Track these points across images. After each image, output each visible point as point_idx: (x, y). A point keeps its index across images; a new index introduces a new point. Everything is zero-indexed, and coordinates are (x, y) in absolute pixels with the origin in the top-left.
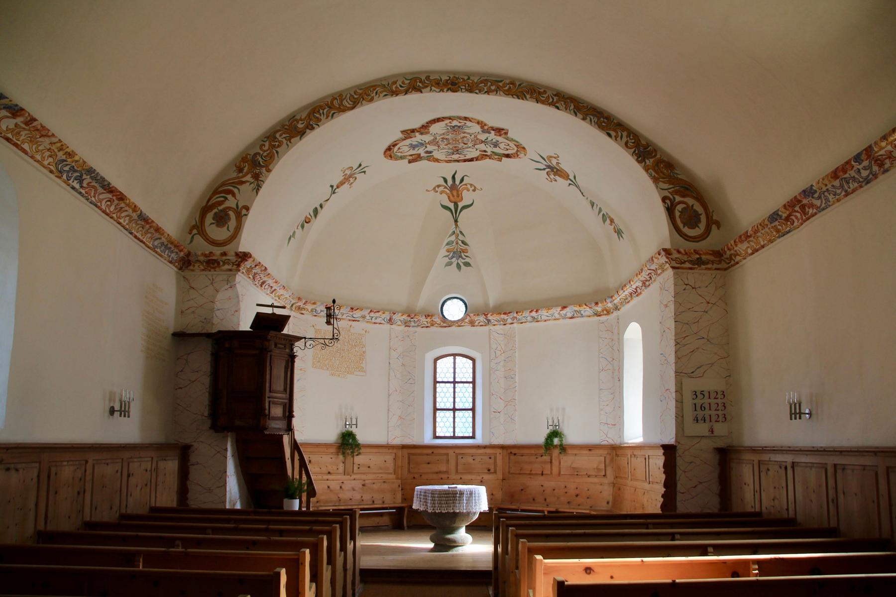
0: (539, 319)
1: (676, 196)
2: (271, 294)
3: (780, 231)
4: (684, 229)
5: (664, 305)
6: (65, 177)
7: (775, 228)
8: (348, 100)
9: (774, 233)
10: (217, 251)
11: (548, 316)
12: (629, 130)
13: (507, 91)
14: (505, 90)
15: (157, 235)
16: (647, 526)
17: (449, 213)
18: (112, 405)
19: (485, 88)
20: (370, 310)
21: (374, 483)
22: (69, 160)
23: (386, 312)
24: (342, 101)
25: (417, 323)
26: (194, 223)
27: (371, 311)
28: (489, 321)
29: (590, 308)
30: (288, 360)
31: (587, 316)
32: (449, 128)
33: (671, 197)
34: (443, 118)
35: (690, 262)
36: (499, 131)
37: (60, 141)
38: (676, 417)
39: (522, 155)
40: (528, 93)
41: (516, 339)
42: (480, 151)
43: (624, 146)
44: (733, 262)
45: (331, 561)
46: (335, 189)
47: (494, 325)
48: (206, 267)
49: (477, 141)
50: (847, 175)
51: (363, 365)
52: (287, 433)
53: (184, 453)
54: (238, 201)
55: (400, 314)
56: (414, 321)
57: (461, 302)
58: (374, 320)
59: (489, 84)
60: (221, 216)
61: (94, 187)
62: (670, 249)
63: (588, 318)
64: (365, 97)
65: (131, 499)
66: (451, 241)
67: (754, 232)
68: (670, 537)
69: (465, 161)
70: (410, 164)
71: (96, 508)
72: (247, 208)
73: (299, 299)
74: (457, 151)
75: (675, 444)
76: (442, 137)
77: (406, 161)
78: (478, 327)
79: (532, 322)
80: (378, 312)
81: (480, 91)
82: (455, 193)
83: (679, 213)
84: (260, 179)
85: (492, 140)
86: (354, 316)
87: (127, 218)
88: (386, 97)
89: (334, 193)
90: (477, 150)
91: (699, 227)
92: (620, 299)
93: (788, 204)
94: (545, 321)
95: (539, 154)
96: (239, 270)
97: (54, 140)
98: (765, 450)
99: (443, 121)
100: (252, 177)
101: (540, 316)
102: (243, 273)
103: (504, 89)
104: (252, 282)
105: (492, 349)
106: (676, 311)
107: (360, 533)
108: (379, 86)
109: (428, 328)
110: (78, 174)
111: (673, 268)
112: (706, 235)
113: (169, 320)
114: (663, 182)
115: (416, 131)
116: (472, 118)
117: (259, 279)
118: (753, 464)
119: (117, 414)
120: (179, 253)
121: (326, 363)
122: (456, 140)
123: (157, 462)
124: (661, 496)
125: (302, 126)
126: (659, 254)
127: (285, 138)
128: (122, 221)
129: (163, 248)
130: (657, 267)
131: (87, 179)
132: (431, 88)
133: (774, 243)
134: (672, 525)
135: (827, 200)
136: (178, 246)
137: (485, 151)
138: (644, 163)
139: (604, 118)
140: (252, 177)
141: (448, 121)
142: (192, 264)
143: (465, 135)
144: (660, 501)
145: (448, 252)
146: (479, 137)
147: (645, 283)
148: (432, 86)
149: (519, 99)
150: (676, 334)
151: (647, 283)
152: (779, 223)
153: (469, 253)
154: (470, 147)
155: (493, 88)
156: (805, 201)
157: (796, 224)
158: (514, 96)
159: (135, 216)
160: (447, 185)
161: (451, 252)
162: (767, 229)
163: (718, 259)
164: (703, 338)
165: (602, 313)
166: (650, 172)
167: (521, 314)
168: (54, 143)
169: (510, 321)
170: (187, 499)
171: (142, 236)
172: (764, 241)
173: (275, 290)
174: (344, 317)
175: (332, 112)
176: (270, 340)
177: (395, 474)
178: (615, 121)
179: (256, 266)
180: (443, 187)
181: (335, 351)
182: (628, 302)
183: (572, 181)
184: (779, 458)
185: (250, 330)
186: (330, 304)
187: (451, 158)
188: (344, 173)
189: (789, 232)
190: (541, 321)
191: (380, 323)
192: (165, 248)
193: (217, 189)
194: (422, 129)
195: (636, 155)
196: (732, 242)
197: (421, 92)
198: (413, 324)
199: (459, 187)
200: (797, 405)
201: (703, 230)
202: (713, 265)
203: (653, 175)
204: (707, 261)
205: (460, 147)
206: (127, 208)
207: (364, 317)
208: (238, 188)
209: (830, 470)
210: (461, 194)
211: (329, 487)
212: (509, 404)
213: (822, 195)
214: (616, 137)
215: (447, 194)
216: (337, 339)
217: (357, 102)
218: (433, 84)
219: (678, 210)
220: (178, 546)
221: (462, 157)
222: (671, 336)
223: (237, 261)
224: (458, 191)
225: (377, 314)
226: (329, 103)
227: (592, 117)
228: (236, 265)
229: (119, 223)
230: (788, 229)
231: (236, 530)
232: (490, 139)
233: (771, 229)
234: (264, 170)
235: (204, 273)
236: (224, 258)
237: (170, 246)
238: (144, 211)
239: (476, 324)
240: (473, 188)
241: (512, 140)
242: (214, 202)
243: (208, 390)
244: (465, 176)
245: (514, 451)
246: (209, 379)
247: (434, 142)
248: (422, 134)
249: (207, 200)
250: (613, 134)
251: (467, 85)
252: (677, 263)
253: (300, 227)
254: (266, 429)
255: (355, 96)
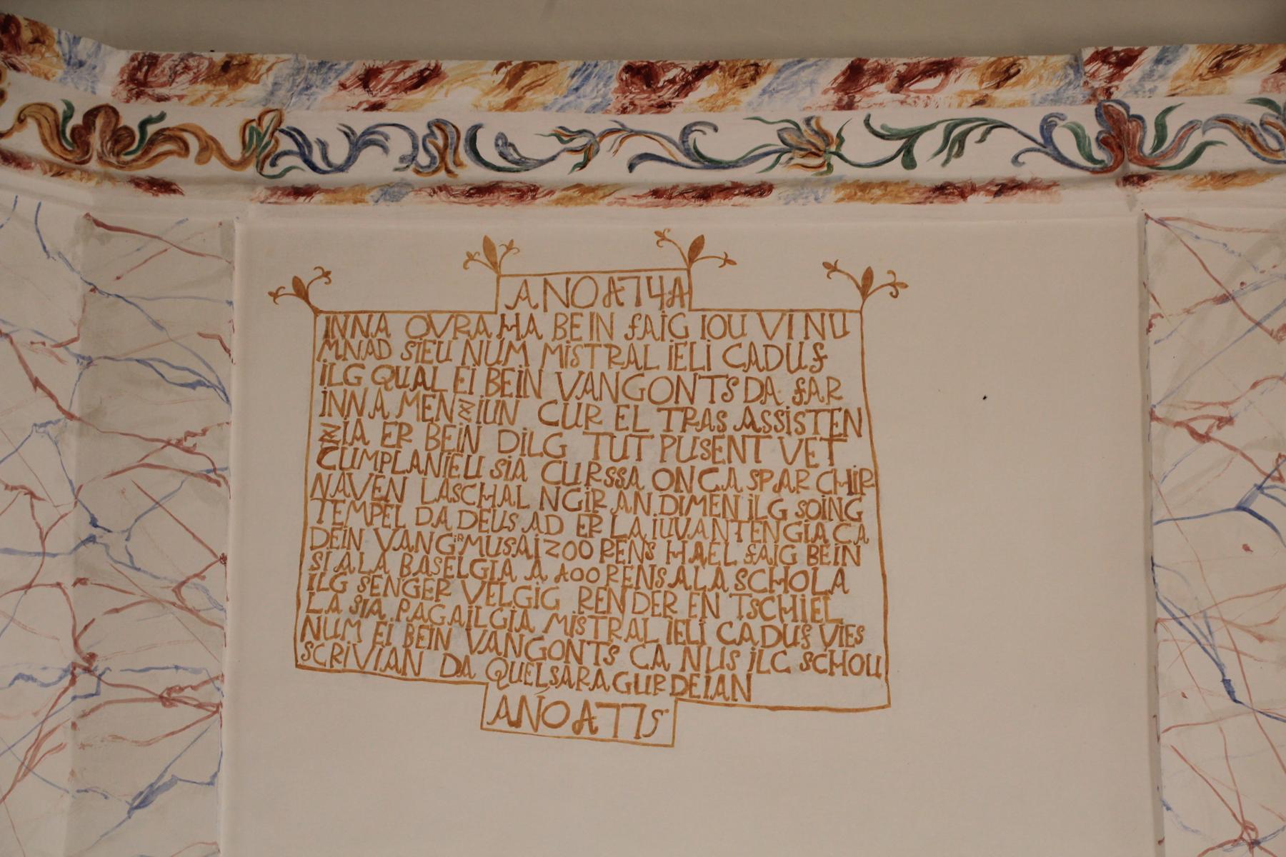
23: (1031, 64)
27: (855, 76)
58: (930, 168)
80: (942, 67)
86: (707, 144)
174: (608, 166)
181: (531, 492)
191: (1004, 188)
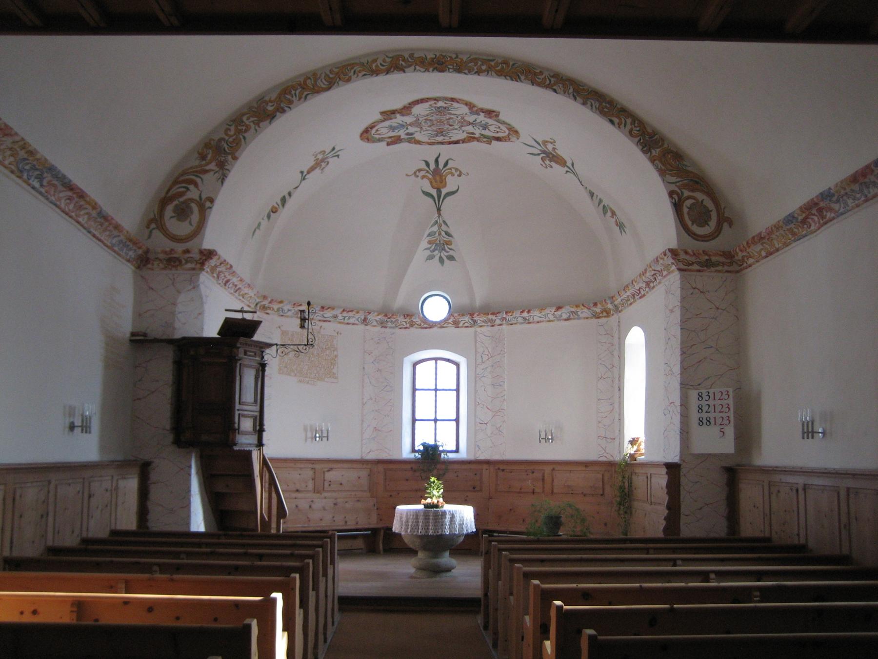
0: (531, 320)
1: (684, 191)
2: (235, 293)
3: (796, 234)
4: (693, 226)
5: (670, 310)
6: (25, 176)
7: (791, 230)
8: (323, 80)
9: (790, 236)
10: (179, 248)
11: (541, 317)
12: (634, 116)
13: (499, 71)
14: (497, 71)
15: (116, 233)
16: (647, 551)
17: (430, 200)
18: (72, 420)
19: (475, 68)
20: (342, 309)
21: (346, 502)
22: (31, 158)
23: (361, 312)
24: (316, 81)
25: (395, 323)
26: (152, 216)
28: (475, 322)
29: (588, 308)
30: (259, 369)
31: (584, 318)
32: (434, 109)
33: (679, 191)
34: (428, 99)
35: (699, 263)
36: (489, 113)
37: (23, 139)
38: (680, 432)
39: (513, 138)
40: (522, 73)
41: (505, 343)
42: (467, 133)
43: (628, 135)
44: (745, 265)
45: (316, 588)
46: (306, 175)
47: (481, 326)
48: (166, 266)
49: (464, 123)
50: (866, 180)
51: (334, 371)
52: (257, 449)
53: (144, 470)
54: (201, 192)
55: (376, 314)
56: (392, 321)
57: (445, 300)
58: (346, 321)
59: (480, 63)
60: (182, 209)
61: (55, 186)
62: (677, 249)
63: (586, 320)
64: (342, 76)
65: (92, 523)
66: (433, 231)
67: (768, 234)
68: (672, 563)
69: (450, 143)
70: (389, 147)
71: (58, 532)
72: (212, 201)
73: (265, 297)
74: (441, 132)
75: (679, 462)
76: (425, 118)
77: (384, 143)
78: (462, 329)
79: (522, 323)
80: (352, 311)
81: (470, 71)
82: (438, 178)
83: (688, 210)
84: (226, 167)
85: (481, 122)
86: (325, 316)
87: (86, 217)
88: (365, 77)
89: (304, 179)
90: (463, 132)
91: (708, 225)
92: (622, 300)
93: (805, 207)
94: (538, 322)
95: (533, 139)
96: (204, 270)
97: (17, 138)
98: (775, 470)
99: (427, 101)
100: (217, 165)
101: (532, 317)
102: (207, 272)
103: (497, 69)
104: (215, 281)
105: (479, 353)
106: (682, 315)
107: (339, 557)
108: (357, 64)
109: (407, 329)
110: (38, 173)
111: (680, 270)
112: (716, 234)
113: (126, 326)
114: (671, 175)
115: (396, 112)
116: (460, 100)
117: (224, 277)
118: (763, 485)
119: (78, 431)
120: (137, 250)
121: (294, 368)
122: (441, 121)
123: (117, 481)
124: (663, 518)
125: (273, 108)
126: (665, 255)
127: (253, 122)
128: (80, 219)
129: (121, 245)
130: (662, 268)
131: (48, 177)
132: (415, 67)
133: (790, 247)
134: (674, 551)
135: (846, 204)
136: (136, 243)
137: (473, 133)
138: (649, 154)
139: (606, 103)
140: (217, 165)
141: (432, 102)
142: (151, 262)
143: (452, 116)
144: (662, 524)
145: (430, 244)
146: (467, 118)
147: (649, 285)
148: (417, 64)
149: (512, 80)
150: (682, 342)
151: (652, 285)
152: (794, 226)
153: (453, 245)
154: (456, 129)
155: (484, 68)
156: (822, 204)
157: (813, 228)
158: (508, 77)
159: (94, 213)
160: (429, 169)
161: (433, 243)
162: (782, 232)
163: (728, 261)
164: (712, 347)
165: (601, 315)
166: (657, 163)
167: (511, 314)
168: (17, 142)
169: (498, 322)
170: (147, 521)
171: (100, 234)
172: (779, 244)
173: (239, 288)
175: (306, 93)
176: (239, 348)
177: (370, 491)
178: (619, 106)
179: (221, 264)
180: (425, 171)
182: (631, 304)
183: (569, 168)
184: (790, 479)
185: (219, 336)
186: (304, 307)
187: (435, 140)
188: (315, 157)
189: (806, 236)
190: (533, 323)
191: (354, 324)
192: (123, 245)
193: (178, 178)
194: (403, 111)
195: (641, 144)
196: (745, 243)
197: (404, 72)
198: (390, 324)
199: (443, 171)
200: (810, 424)
201: (713, 228)
202: (723, 266)
203: (659, 167)
204: (718, 263)
205: (445, 129)
206: (87, 206)
207: (335, 317)
208: (200, 177)
209: (843, 494)
210: (445, 179)
211: (297, 506)
212: (496, 414)
213: (841, 199)
214: (619, 124)
215: (429, 179)
216: (312, 345)
217: (333, 82)
218: (418, 62)
219: (686, 206)
220: (156, 571)
221: (447, 139)
222: (676, 344)
223: (201, 259)
224: (441, 176)
225: (351, 314)
226: (302, 82)
227: (593, 102)
228: (200, 263)
229: (78, 222)
230: (805, 232)
231: (212, 554)
232: (478, 121)
233: (787, 232)
234: (229, 158)
235: (165, 272)
236: (188, 255)
237: (128, 243)
238: (104, 208)
239: (461, 325)
240: (458, 173)
241: (504, 123)
242: (174, 192)
243: (170, 401)
244: (449, 159)
245: (502, 467)
246: (171, 388)
247: (417, 123)
248: (403, 115)
249: (166, 189)
250: (616, 120)
251: (455, 64)
252: (684, 265)
253: (266, 218)
254: (235, 444)
255: (331, 76)
